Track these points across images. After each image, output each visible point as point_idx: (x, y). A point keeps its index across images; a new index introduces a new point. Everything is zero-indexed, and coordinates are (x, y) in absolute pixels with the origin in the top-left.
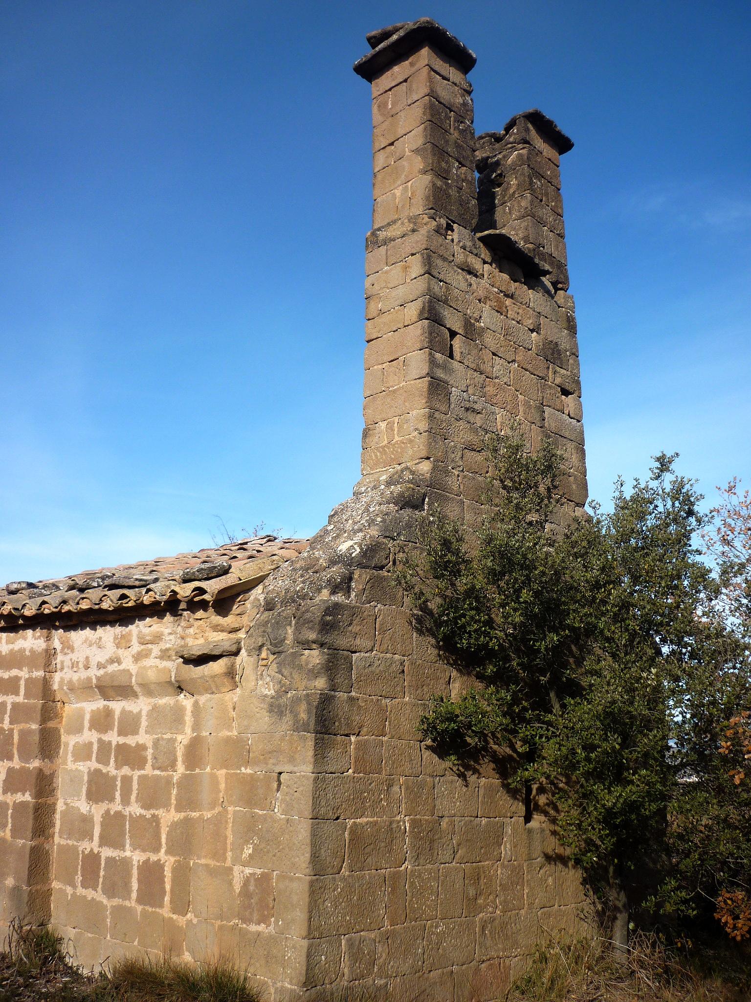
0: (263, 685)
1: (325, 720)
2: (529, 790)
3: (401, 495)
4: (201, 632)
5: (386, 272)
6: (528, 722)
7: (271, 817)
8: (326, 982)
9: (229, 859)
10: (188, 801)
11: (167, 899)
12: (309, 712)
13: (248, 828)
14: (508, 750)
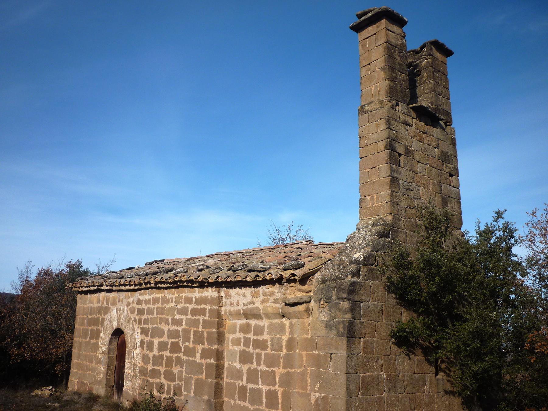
2: (437, 362)
3: (380, 232)
4: (293, 292)
5: (368, 126)
6: (437, 332)
7: (328, 372)
12: (344, 328)
13: (317, 377)
14: (428, 344)
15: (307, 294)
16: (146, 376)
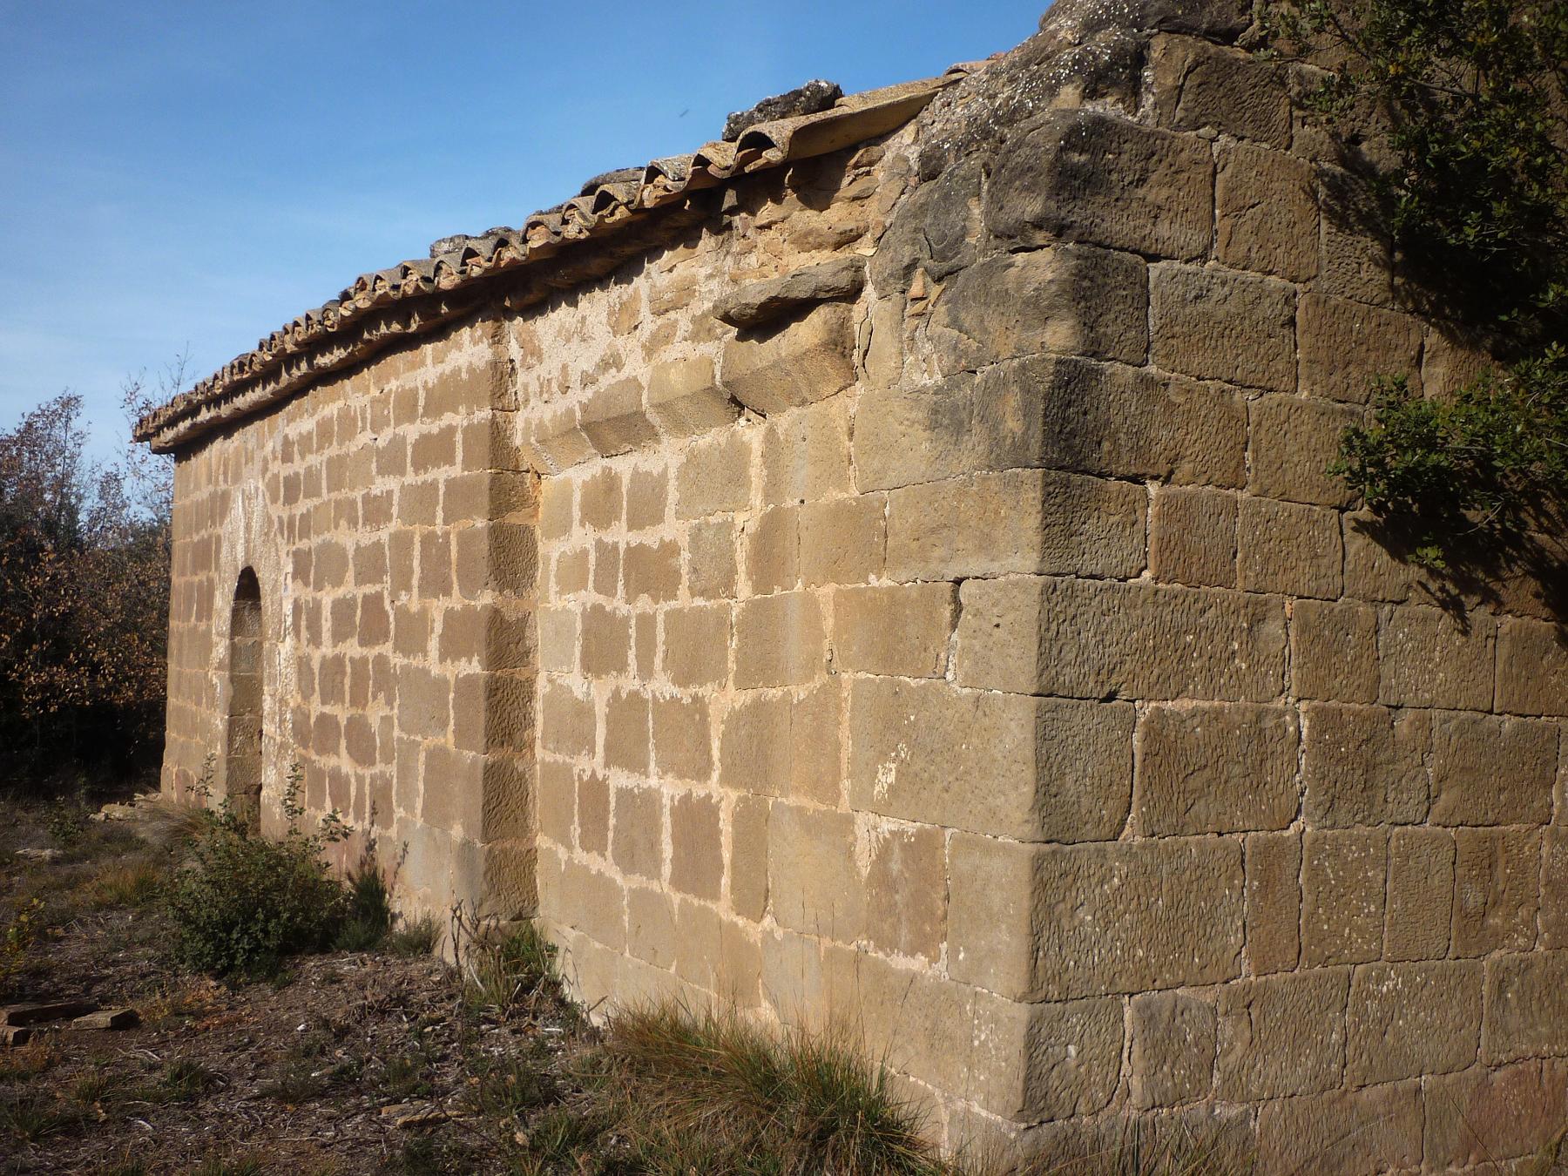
0: (916, 364)
1: (1073, 434)
4: (773, 249)
8: (1081, 1108)
9: (845, 795)
10: (760, 667)
11: (725, 880)
15: (844, 255)
16: (306, 747)
